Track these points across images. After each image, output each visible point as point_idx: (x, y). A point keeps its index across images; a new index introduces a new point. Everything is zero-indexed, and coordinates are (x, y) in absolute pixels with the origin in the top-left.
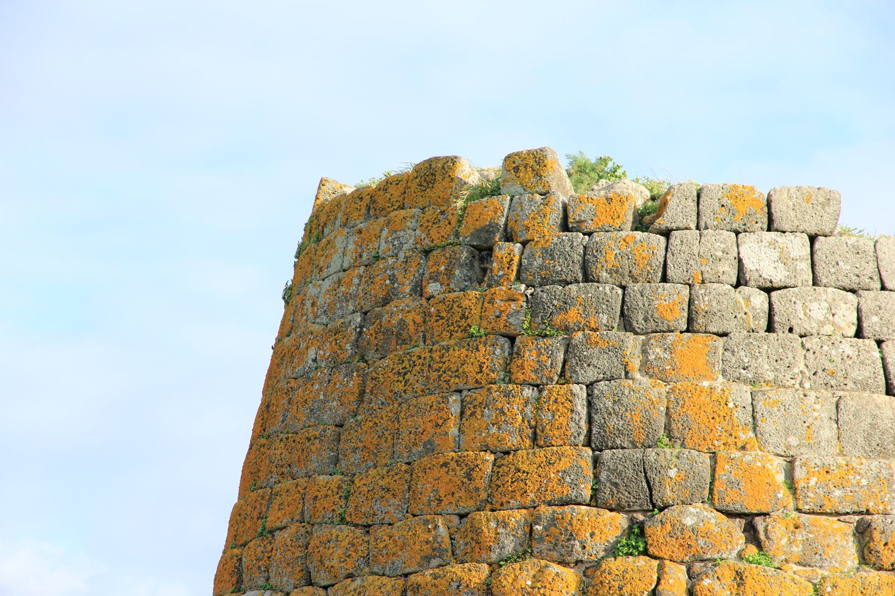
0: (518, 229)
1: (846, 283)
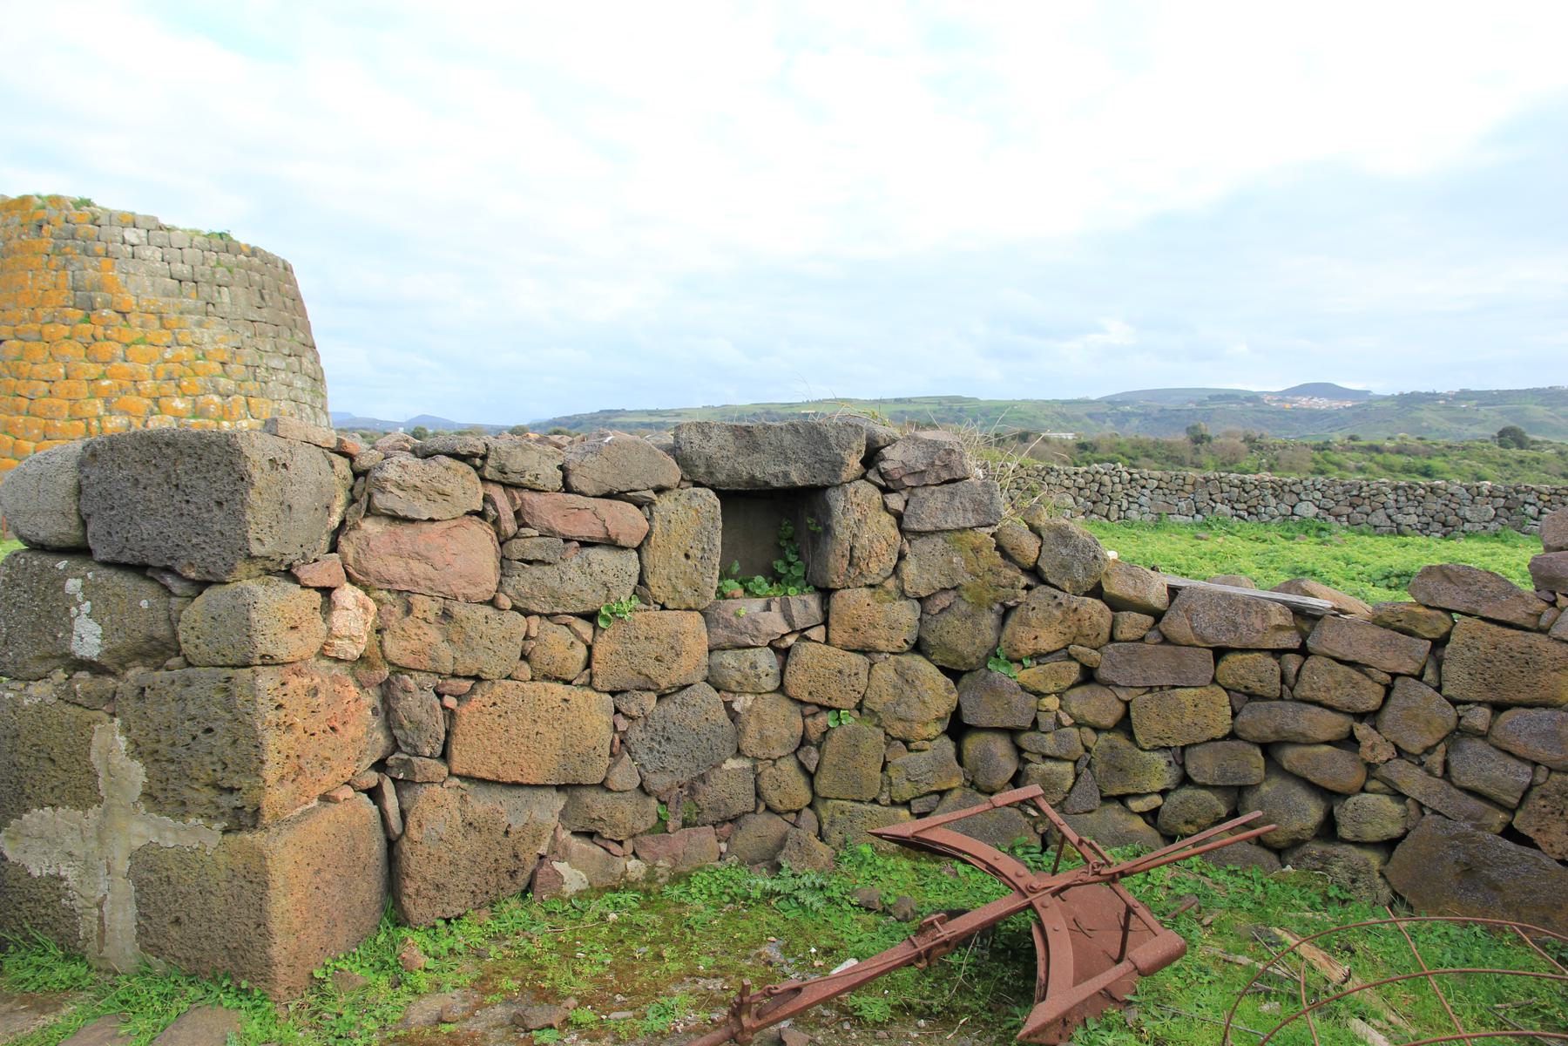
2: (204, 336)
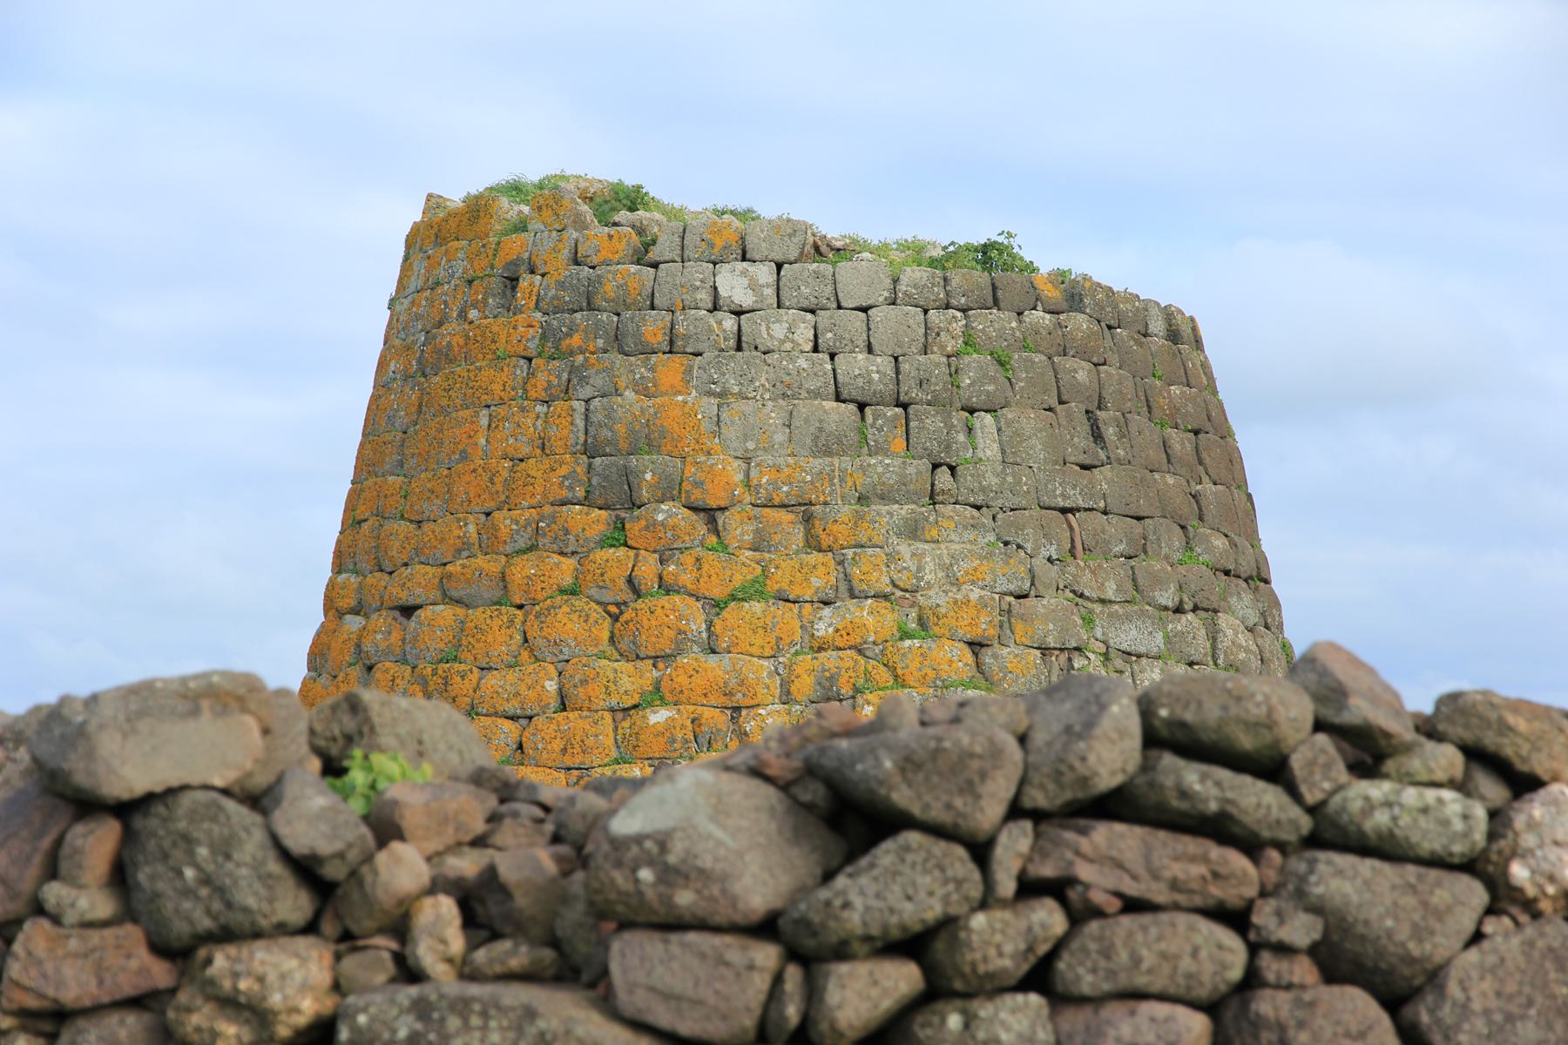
0: (538, 262)
1: (805, 304)
2: (924, 562)
